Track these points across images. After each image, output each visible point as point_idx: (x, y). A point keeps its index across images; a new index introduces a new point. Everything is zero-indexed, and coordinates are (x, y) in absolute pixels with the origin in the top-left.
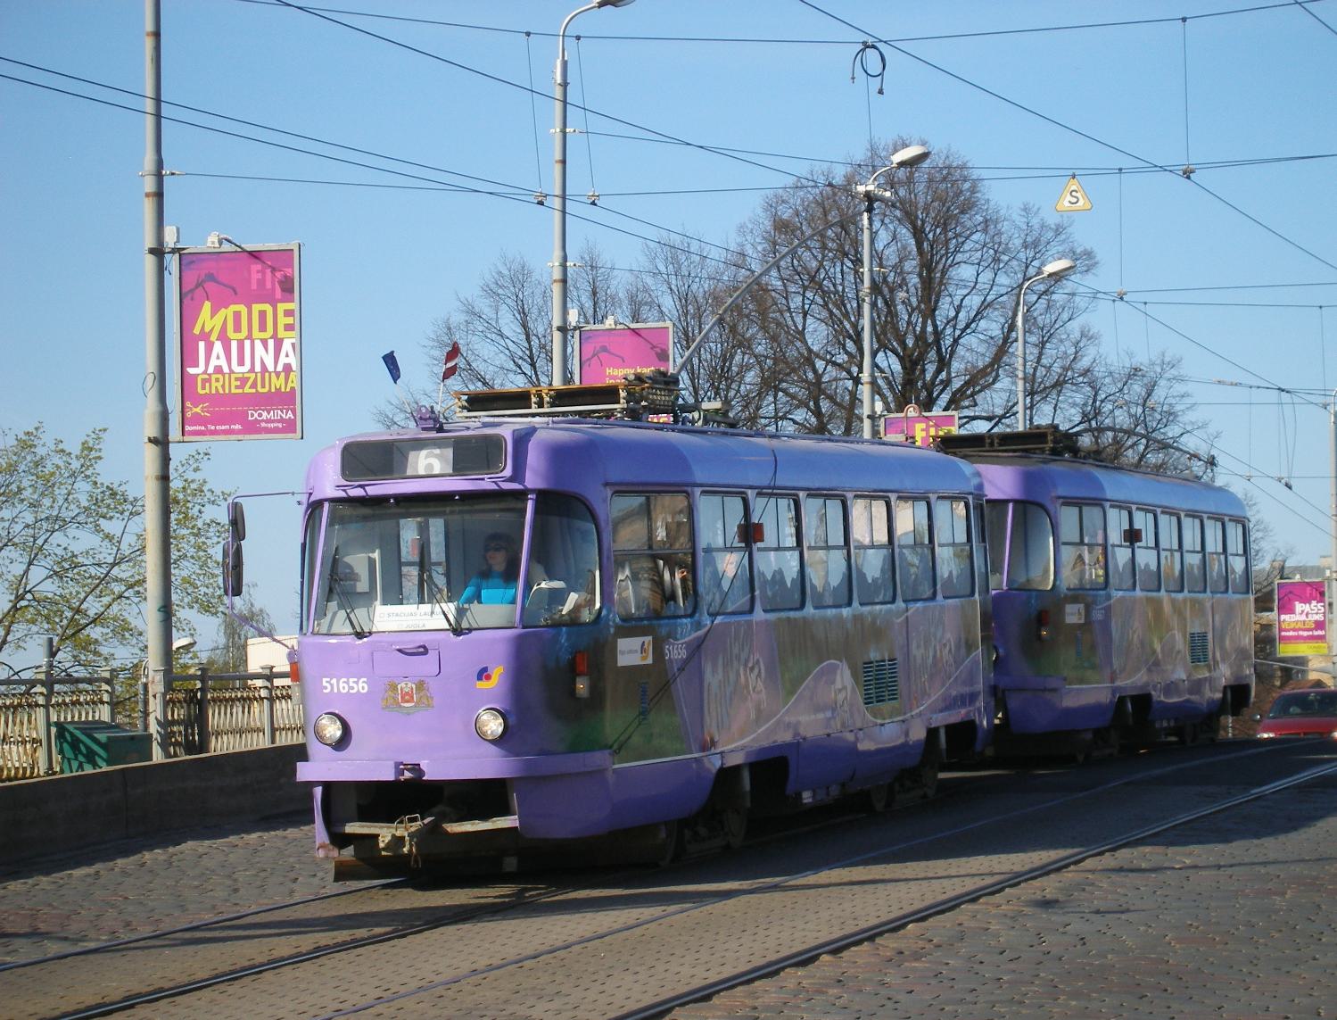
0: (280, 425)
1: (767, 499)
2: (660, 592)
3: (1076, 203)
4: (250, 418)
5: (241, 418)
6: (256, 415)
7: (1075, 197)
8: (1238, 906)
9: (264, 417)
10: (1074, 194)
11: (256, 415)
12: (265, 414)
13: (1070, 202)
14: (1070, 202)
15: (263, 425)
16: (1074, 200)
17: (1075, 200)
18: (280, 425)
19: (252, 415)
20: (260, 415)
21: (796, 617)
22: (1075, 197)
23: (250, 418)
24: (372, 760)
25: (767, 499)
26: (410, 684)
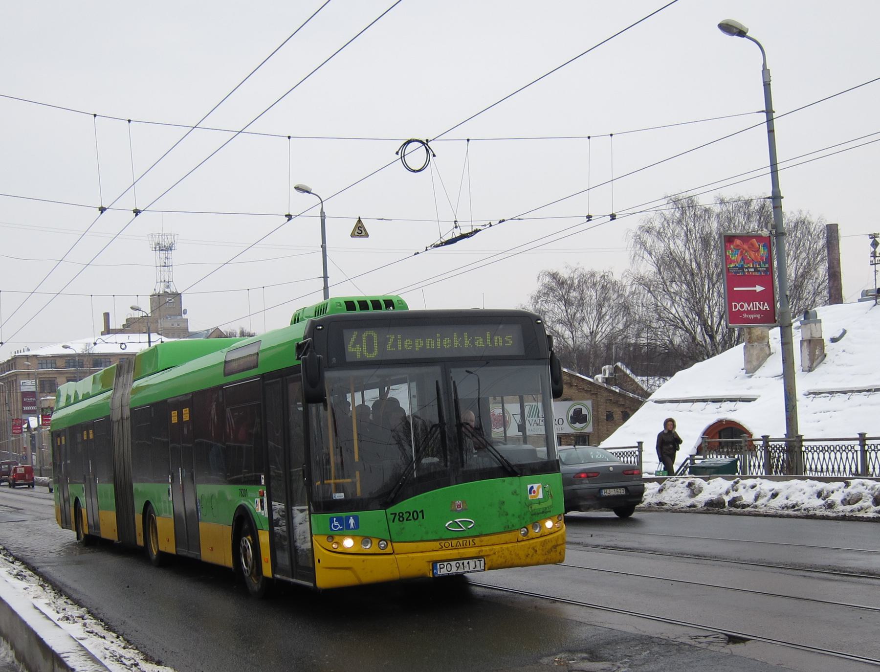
0: (758, 316)
1: (266, 332)
2: (40, 570)
3: (360, 234)
4: (734, 310)
5: (720, 296)
6: (738, 307)
7: (360, 230)
8: (562, 663)
9: (745, 308)
10: (360, 228)
11: (738, 307)
12: (746, 305)
13: (358, 233)
14: (358, 233)
15: (745, 316)
16: (360, 232)
17: (360, 232)
18: (758, 316)
19: (736, 307)
20: (742, 306)
21: (354, 441)
22: (360, 230)
23: (734, 310)
24: (187, 533)
25: (266, 332)
26: (460, 502)
